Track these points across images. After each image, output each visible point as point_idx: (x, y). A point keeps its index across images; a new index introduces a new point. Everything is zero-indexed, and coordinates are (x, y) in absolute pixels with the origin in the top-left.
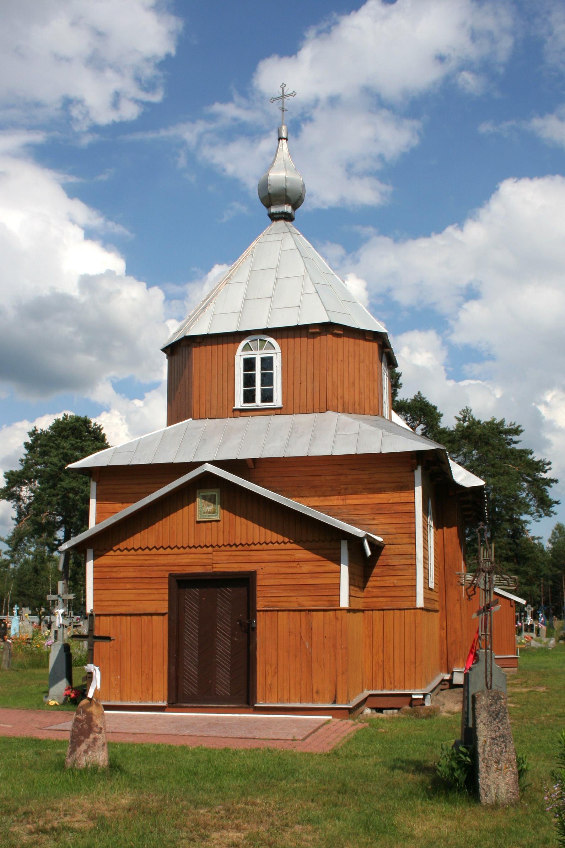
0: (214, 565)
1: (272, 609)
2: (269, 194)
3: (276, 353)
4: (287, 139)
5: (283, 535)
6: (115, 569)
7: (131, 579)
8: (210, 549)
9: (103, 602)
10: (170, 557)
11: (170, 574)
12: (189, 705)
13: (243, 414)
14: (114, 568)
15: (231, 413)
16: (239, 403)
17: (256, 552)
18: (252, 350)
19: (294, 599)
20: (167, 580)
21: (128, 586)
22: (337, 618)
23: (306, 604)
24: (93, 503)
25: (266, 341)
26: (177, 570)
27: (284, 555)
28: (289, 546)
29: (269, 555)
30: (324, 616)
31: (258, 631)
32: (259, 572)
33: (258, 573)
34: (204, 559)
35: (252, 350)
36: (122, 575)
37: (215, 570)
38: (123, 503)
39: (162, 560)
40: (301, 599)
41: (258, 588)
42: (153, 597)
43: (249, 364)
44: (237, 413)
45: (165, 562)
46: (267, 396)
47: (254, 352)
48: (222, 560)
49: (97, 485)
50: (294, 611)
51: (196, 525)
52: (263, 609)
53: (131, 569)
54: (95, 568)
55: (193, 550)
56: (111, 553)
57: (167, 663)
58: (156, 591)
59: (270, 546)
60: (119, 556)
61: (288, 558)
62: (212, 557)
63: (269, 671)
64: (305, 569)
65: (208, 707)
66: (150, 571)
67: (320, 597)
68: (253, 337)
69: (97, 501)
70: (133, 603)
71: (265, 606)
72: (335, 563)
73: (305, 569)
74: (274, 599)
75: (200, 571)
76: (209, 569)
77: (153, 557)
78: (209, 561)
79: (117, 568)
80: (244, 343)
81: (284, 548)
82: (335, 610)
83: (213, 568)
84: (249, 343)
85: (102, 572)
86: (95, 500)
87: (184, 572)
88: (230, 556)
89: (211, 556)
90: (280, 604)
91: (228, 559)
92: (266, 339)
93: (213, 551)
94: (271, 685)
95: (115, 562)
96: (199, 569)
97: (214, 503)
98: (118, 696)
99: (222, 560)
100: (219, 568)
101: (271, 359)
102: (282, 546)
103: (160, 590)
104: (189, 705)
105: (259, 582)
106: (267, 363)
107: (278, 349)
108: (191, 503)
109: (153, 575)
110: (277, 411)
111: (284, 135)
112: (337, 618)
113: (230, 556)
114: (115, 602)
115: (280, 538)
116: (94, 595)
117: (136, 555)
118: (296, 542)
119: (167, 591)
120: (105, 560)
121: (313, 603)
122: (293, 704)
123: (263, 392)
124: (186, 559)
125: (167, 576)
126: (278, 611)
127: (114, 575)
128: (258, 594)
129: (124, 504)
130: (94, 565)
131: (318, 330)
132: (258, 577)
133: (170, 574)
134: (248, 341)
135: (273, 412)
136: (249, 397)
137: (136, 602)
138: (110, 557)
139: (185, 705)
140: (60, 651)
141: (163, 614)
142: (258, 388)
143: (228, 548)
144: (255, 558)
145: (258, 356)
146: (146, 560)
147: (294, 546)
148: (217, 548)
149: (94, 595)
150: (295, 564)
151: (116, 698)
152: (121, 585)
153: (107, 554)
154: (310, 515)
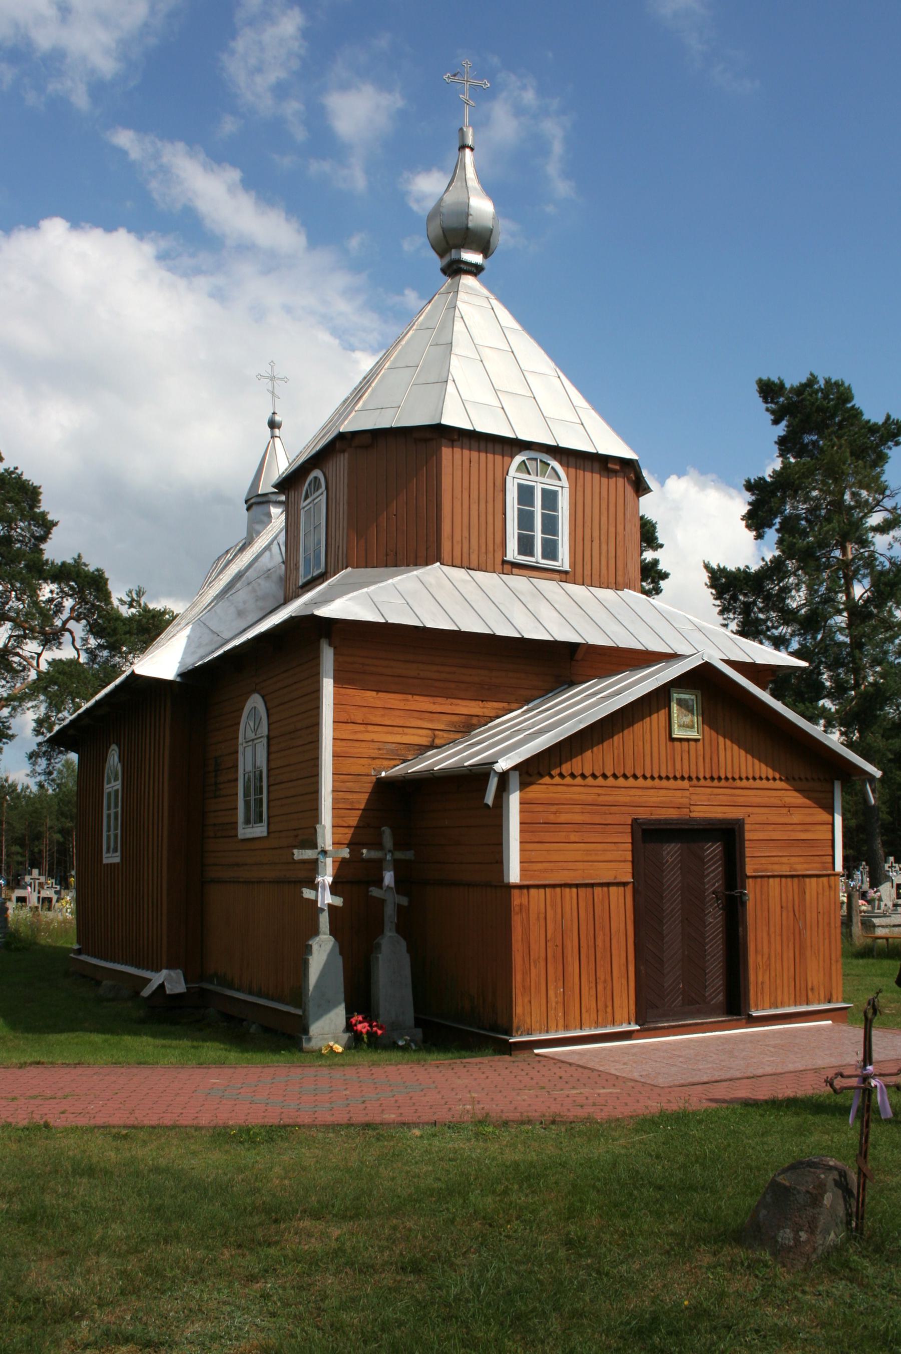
0: (693, 808)
1: (763, 874)
2: (467, 228)
3: (562, 487)
4: (472, 149)
5: (774, 769)
6: (554, 808)
7: (576, 826)
8: (686, 783)
9: (534, 864)
10: (633, 792)
11: (635, 820)
12: (666, 1024)
13: (515, 571)
14: (551, 806)
15: (499, 567)
16: (512, 552)
17: (742, 791)
18: (537, 475)
19: (785, 860)
20: (628, 829)
21: (573, 837)
22: (830, 887)
23: (798, 867)
24: (328, 686)
25: (549, 465)
26: (643, 814)
27: (772, 798)
28: (779, 784)
29: (756, 796)
30: (817, 884)
31: (750, 905)
32: (747, 820)
33: (746, 822)
34: (679, 798)
35: (537, 475)
36: (563, 818)
37: (693, 815)
38: (378, 691)
39: (622, 797)
40: (793, 860)
41: (747, 844)
42: (609, 856)
43: (526, 494)
44: (507, 568)
45: (627, 799)
46: (550, 551)
47: (533, 477)
48: (701, 801)
49: (335, 654)
50: (786, 876)
51: (668, 743)
52: (754, 874)
53: (577, 808)
54: (522, 806)
55: (664, 783)
56: (547, 780)
57: (633, 962)
58: (612, 846)
59: (758, 784)
60: (559, 787)
61: (777, 802)
62: (688, 795)
63: (761, 964)
64: (795, 819)
65: (663, 1028)
66: (605, 813)
67: (812, 858)
68: (533, 454)
69: (335, 682)
70: (580, 865)
71: (755, 870)
72: (825, 811)
73: (797, 817)
74: (763, 860)
75: (675, 817)
76: (684, 814)
77: (608, 791)
78: (685, 801)
79: (555, 806)
80: (518, 459)
81: (774, 787)
82: (828, 875)
83: (690, 812)
84: (526, 461)
85: (533, 812)
86: (332, 681)
87: (653, 817)
88: (711, 795)
89: (687, 793)
90: (770, 867)
91: (709, 800)
92: (549, 462)
93: (691, 786)
94: (762, 983)
95: (551, 795)
96: (671, 814)
97: (692, 712)
98: (561, 1022)
99: (701, 801)
100: (700, 813)
101: (555, 493)
102: (771, 784)
103: (620, 845)
104: (666, 1024)
105: (748, 835)
106: (550, 498)
107: (565, 482)
108: (661, 710)
109: (610, 819)
110: (564, 576)
111: (470, 142)
112: (830, 887)
113: (711, 795)
114: (552, 864)
115: (771, 773)
116: (521, 850)
117: (584, 786)
118: (787, 780)
119: (629, 846)
120: (537, 791)
121: (805, 866)
122: (787, 1008)
123: (545, 542)
124: (654, 797)
125: (630, 822)
126: (769, 877)
127: (552, 818)
128: (748, 852)
129: (380, 694)
130: (521, 798)
131: (617, 467)
132: (747, 827)
133: (635, 820)
134: (524, 458)
135: (557, 576)
136: (526, 546)
137: (586, 864)
138: (545, 786)
139: (660, 1025)
140: (330, 955)
141: (624, 884)
142: (538, 536)
143: (709, 783)
144: (741, 800)
145: (539, 483)
146: (599, 795)
147: (783, 785)
148: (695, 782)
149: (522, 850)
150: (785, 810)
151: (557, 1026)
152: (562, 836)
153: (540, 782)
154: (562, 738)
